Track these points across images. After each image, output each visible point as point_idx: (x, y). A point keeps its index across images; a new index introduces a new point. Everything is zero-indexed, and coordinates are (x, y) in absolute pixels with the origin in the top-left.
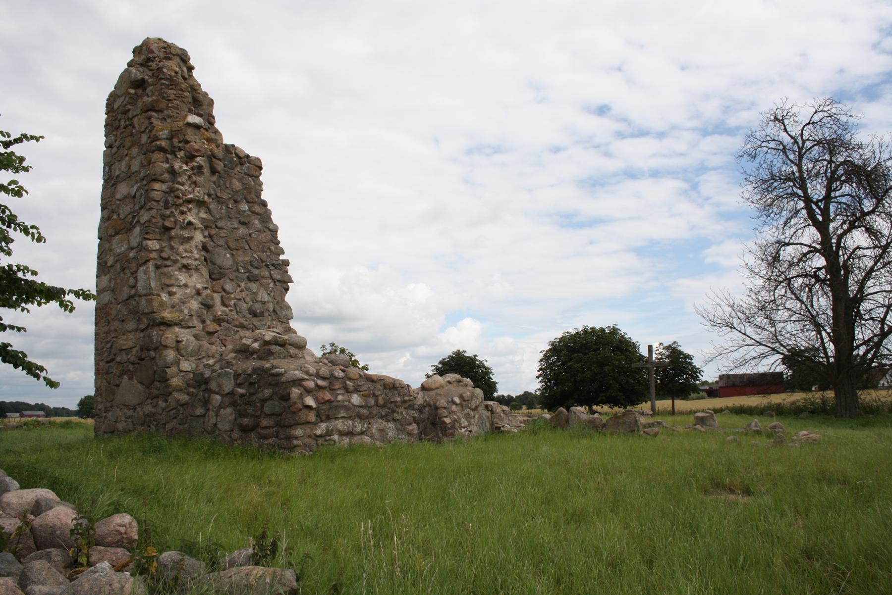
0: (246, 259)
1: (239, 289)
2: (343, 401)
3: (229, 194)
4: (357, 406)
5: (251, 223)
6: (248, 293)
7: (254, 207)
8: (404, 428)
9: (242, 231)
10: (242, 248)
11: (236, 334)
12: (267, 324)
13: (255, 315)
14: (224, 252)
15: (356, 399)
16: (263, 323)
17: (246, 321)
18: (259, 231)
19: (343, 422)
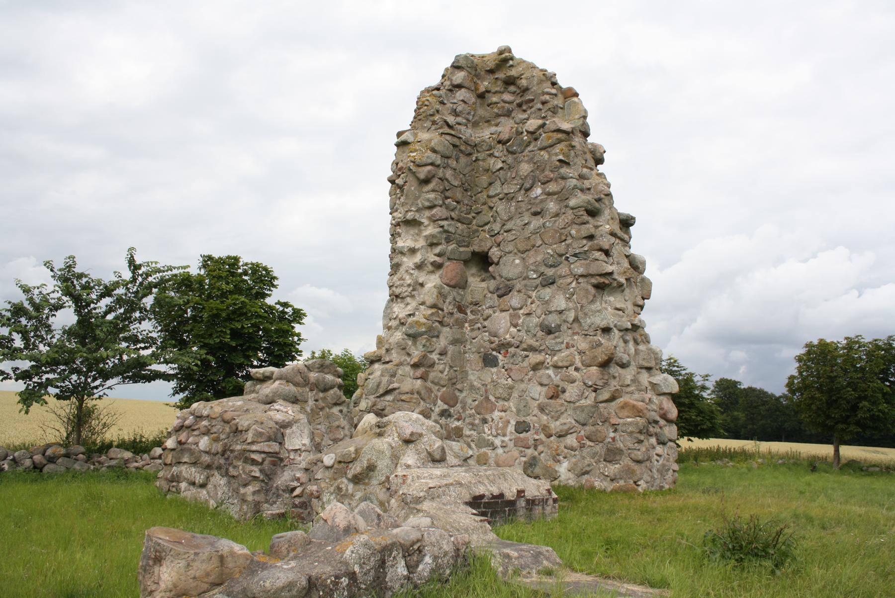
0: (538, 259)
1: (530, 300)
3: (516, 184)
5: (545, 209)
9: (536, 223)
10: (534, 246)
11: (523, 361)
13: (549, 332)
16: (558, 340)
18: (557, 215)
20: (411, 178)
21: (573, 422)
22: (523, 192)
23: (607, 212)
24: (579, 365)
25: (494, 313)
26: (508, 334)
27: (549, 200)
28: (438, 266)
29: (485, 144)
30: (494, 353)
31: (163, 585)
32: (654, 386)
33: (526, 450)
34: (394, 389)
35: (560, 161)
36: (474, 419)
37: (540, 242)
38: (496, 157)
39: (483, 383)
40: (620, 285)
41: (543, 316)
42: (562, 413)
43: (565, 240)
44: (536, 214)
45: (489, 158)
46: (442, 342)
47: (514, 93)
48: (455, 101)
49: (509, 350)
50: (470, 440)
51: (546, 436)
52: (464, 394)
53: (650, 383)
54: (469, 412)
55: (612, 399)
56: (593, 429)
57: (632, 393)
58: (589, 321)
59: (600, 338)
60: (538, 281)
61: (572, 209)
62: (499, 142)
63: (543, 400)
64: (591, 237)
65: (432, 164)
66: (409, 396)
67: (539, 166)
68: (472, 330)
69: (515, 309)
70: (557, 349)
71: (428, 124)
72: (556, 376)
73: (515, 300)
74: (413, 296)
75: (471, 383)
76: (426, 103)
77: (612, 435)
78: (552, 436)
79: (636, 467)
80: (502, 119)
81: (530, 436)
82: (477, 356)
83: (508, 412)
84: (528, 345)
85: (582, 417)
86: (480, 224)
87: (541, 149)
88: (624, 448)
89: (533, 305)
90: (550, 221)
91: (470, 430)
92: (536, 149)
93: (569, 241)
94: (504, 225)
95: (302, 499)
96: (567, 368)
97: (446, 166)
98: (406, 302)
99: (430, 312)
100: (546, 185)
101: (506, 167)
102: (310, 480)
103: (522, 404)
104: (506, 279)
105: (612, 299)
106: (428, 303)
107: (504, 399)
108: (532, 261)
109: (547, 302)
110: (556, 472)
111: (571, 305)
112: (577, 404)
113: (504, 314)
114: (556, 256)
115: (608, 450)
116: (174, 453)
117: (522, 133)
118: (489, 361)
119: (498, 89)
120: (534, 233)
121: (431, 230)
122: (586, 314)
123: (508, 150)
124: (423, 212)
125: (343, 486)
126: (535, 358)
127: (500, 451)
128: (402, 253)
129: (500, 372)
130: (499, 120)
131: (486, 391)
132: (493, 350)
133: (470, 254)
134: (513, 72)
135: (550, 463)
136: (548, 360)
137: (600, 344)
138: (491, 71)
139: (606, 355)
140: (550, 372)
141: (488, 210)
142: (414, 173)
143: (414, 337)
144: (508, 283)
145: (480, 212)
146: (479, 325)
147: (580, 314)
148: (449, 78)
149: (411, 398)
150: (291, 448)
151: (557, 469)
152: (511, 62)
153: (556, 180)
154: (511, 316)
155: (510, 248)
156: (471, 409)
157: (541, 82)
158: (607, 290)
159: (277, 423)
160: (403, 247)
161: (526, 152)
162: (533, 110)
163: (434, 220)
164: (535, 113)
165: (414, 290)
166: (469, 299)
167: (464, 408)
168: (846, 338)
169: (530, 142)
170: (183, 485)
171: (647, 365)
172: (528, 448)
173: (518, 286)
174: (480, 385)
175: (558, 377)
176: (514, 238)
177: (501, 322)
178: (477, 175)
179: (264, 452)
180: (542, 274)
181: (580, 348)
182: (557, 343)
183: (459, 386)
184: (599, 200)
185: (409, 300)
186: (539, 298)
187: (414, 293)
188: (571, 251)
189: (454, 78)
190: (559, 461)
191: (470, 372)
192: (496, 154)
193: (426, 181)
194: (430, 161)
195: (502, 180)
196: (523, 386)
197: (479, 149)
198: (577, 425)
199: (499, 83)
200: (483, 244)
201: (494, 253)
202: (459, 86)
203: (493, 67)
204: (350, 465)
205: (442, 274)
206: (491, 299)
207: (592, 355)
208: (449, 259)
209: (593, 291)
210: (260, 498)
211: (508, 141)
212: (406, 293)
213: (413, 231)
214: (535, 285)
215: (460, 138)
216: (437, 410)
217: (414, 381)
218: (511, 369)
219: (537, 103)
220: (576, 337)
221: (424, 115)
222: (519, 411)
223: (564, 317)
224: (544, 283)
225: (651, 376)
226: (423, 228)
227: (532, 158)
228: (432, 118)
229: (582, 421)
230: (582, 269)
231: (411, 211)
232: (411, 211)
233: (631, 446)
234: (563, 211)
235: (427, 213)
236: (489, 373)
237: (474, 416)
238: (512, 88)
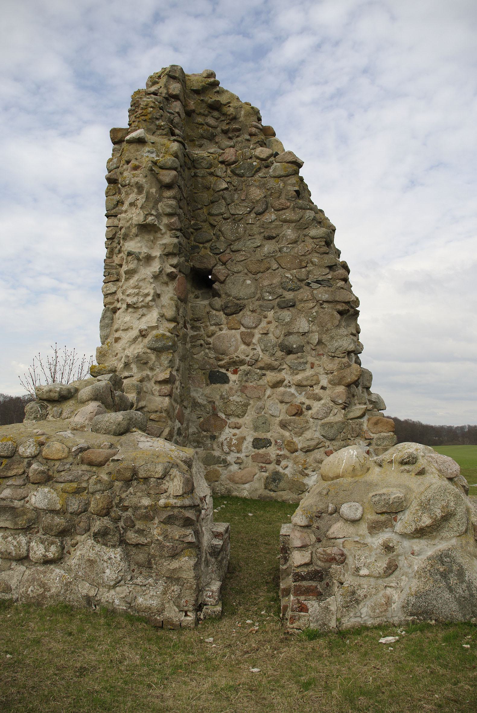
0: (274, 282)
3: (247, 207)
9: (268, 247)
11: (260, 379)
18: (295, 242)
22: (253, 215)
25: (221, 330)
27: (285, 227)
30: (223, 371)
33: (267, 466)
39: (211, 400)
43: (306, 266)
44: (270, 238)
51: (289, 451)
61: (313, 238)
62: (222, 162)
73: (248, 318)
75: (194, 400)
78: (297, 451)
81: (272, 452)
90: (287, 247)
99: (173, 325)
100: (281, 212)
104: (234, 298)
107: (238, 416)
108: (266, 283)
110: (304, 485)
111: (314, 328)
112: (326, 420)
114: (296, 281)
122: (332, 338)
123: (232, 171)
127: (234, 468)
135: (298, 477)
144: (238, 302)
145: (200, 229)
151: (305, 482)
154: (242, 334)
155: (239, 268)
157: (248, 115)
160: (140, 253)
161: (257, 177)
162: (239, 139)
169: (260, 169)
172: (269, 463)
176: (243, 258)
181: (327, 368)
188: (312, 278)
190: (307, 475)
191: (192, 389)
192: (219, 174)
195: (229, 200)
198: (324, 439)
199: (204, 105)
201: (220, 270)
209: (338, 316)
211: (234, 162)
221: (149, 116)
224: (283, 305)
226: (159, 235)
227: (264, 184)
229: (331, 435)
230: (327, 296)
231: (152, 215)
232: (152, 215)
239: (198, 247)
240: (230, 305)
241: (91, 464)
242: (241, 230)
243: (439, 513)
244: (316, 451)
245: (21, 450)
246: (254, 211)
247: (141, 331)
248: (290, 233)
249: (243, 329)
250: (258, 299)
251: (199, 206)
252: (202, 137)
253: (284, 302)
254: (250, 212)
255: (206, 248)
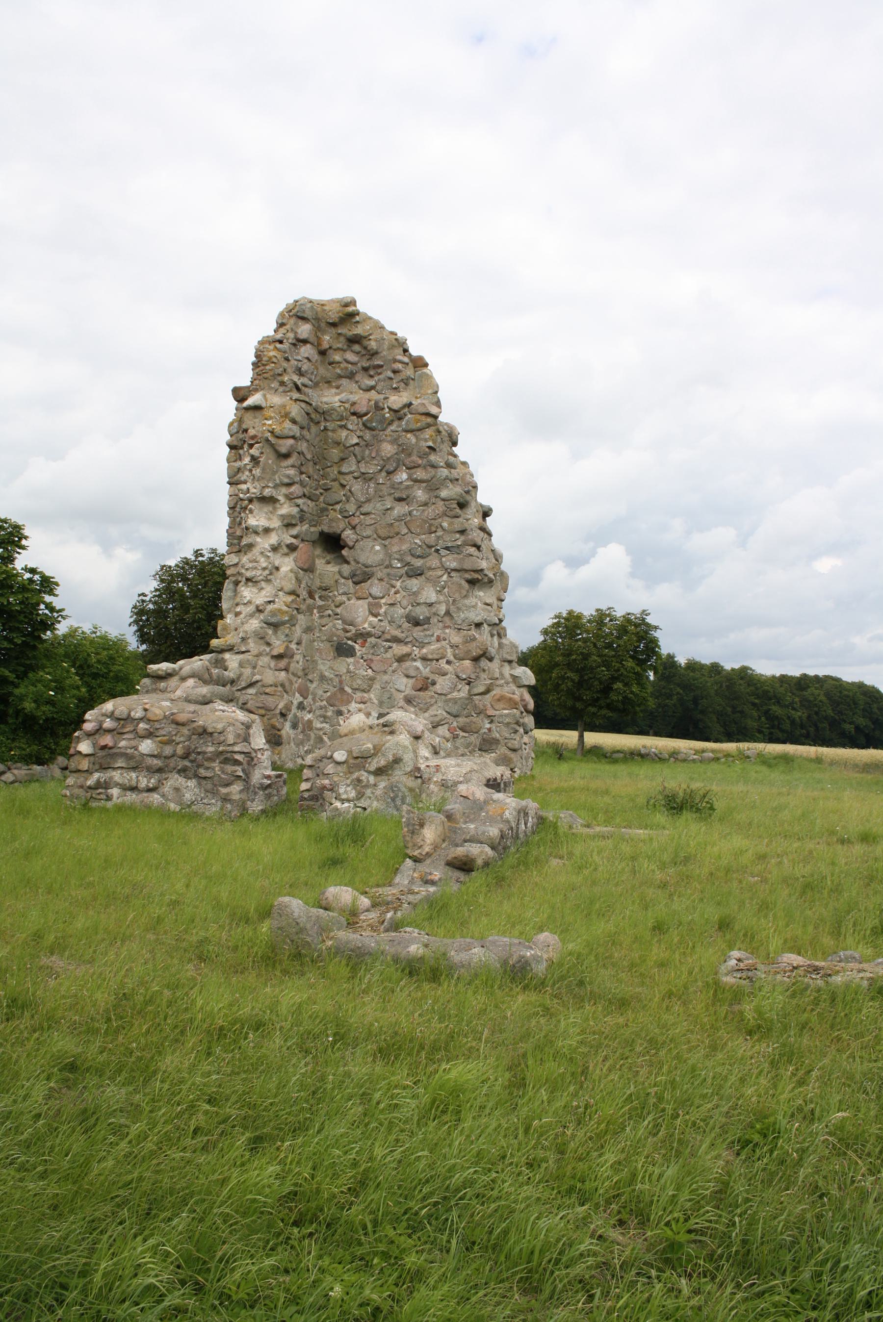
0: (403, 548)
1: (393, 590)
2: (126, 748)
3: (377, 465)
4: (147, 755)
5: (411, 497)
6: (404, 593)
7: (415, 473)
8: (217, 790)
9: (400, 509)
10: (398, 534)
11: (386, 652)
12: (435, 635)
13: (417, 623)
14: (371, 544)
15: (146, 746)
16: (428, 633)
17: (403, 632)
18: (426, 504)
19: (121, 774)
20: (268, 450)
21: (445, 713)
23: (473, 504)
24: (452, 658)
25: (349, 600)
26: (366, 623)
27: (416, 487)
28: (292, 548)
29: (336, 414)
30: (350, 642)
31: (428, 842)
32: (515, 678)
34: (257, 682)
35: (430, 447)
36: (326, 711)
37: (406, 531)
38: (348, 430)
40: (491, 581)
41: (410, 607)
42: (432, 705)
44: (400, 500)
45: (340, 430)
46: (298, 631)
47: (358, 353)
48: (299, 358)
49: (369, 640)
50: (321, 733)
52: (314, 685)
53: (512, 675)
54: (319, 704)
55: (487, 691)
56: (467, 720)
57: (502, 686)
58: (462, 616)
59: (473, 632)
60: (403, 571)
61: (444, 500)
62: (354, 414)
63: (409, 691)
64: (462, 532)
65: (293, 437)
66: (273, 688)
67: (405, 450)
68: (321, 617)
69: (375, 598)
70: (427, 641)
71: (275, 385)
72: (425, 668)
73: (376, 589)
74: (268, 581)
76: (274, 360)
77: (488, 726)
79: (512, 755)
80: (344, 382)
82: (328, 645)
83: (368, 704)
84: (392, 636)
85: (454, 709)
86: (331, 502)
87: (407, 431)
88: (500, 738)
89: (398, 595)
90: (417, 510)
91: (322, 723)
92: (400, 429)
93: (440, 533)
94: (360, 507)
95: (311, 793)
96: (437, 660)
97: (303, 437)
98: (259, 587)
99: (290, 598)
100: (413, 471)
101: (363, 443)
102: (318, 775)
103: (386, 695)
104: (363, 565)
105: (481, 594)
106: (286, 589)
107: (363, 691)
108: (395, 549)
109: (416, 594)
111: (442, 598)
112: (449, 696)
113: (360, 602)
114: (425, 547)
115: (484, 740)
116: (92, 758)
117: (383, 409)
118: (343, 651)
119: (340, 346)
120: (399, 519)
121: (285, 509)
122: (459, 609)
123: (364, 425)
124: (280, 488)
125: (363, 778)
126: (399, 650)
128: (256, 533)
129: (358, 662)
130: (341, 382)
131: (341, 682)
132: (348, 639)
133: (318, 535)
134: (359, 330)
136: (416, 653)
137: (474, 639)
138: (334, 325)
139: (481, 649)
140: (418, 664)
141: (340, 487)
142: (272, 446)
143: (275, 626)
145: (329, 489)
146: (330, 612)
147: (452, 609)
148: (292, 330)
149: (275, 691)
150: (257, 748)
152: (357, 318)
153: (425, 468)
154: (370, 604)
155: (368, 532)
156: (322, 701)
157: (392, 347)
158: (478, 585)
159: (243, 724)
160: (257, 526)
162: (381, 377)
163: (289, 498)
164: (384, 380)
165: (271, 574)
166: (318, 583)
167: (314, 699)
168: (597, 610)
169: (392, 421)
170: (115, 792)
171: (510, 658)
173: (379, 575)
174: (332, 676)
175: (428, 669)
177: (359, 611)
178: (326, 447)
179: (243, 753)
180: (408, 564)
182: (426, 636)
183: (310, 677)
184: (467, 492)
185: (263, 584)
186: (405, 589)
187: (269, 577)
189: (299, 331)
191: (320, 662)
192: (350, 427)
193: (286, 456)
194: (291, 434)
195: (359, 457)
196: (386, 678)
197: (327, 418)
198: (448, 716)
199: (342, 339)
200: (334, 524)
201: (348, 535)
202: (305, 342)
203: (337, 320)
204: (369, 760)
205: (296, 557)
206: (344, 585)
207: (466, 649)
208: (302, 540)
209: (466, 585)
210: (244, 796)
212: (261, 577)
213: (268, 508)
214: (399, 574)
215: (311, 405)
216: (295, 703)
217: (277, 673)
218: (371, 660)
219: (386, 370)
220: (447, 631)
221: (271, 373)
222: (381, 703)
223: (434, 610)
225: (512, 668)
226: (278, 506)
227: (396, 439)
228: (280, 378)
229: (454, 711)
230: (455, 564)
231: (268, 487)
233: (507, 735)
234: (433, 500)
235: (284, 490)
236: (344, 663)
237: (325, 707)
238: (357, 347)
239: (327, 510)
240: (358, 572)
241: (177, 724)
242: (371, 490)
243: (391, 758)
244: (440, 727)
245: (132, 714)
246: (385, 469)
247: (257, 607)
248: (420, 494)
249: (370, 599)
250: (387, 567)
251: (329, 464)
252: (340, 377)
253: (412, 570)
254: (381, 470)
255: (335, 510)
